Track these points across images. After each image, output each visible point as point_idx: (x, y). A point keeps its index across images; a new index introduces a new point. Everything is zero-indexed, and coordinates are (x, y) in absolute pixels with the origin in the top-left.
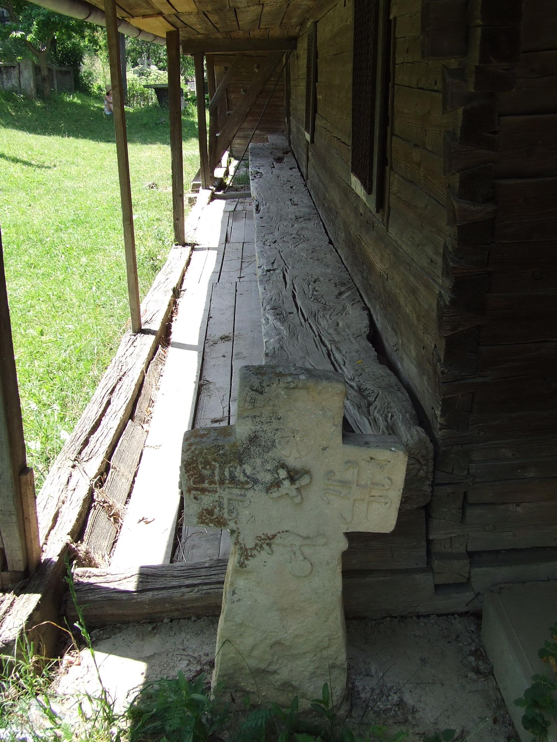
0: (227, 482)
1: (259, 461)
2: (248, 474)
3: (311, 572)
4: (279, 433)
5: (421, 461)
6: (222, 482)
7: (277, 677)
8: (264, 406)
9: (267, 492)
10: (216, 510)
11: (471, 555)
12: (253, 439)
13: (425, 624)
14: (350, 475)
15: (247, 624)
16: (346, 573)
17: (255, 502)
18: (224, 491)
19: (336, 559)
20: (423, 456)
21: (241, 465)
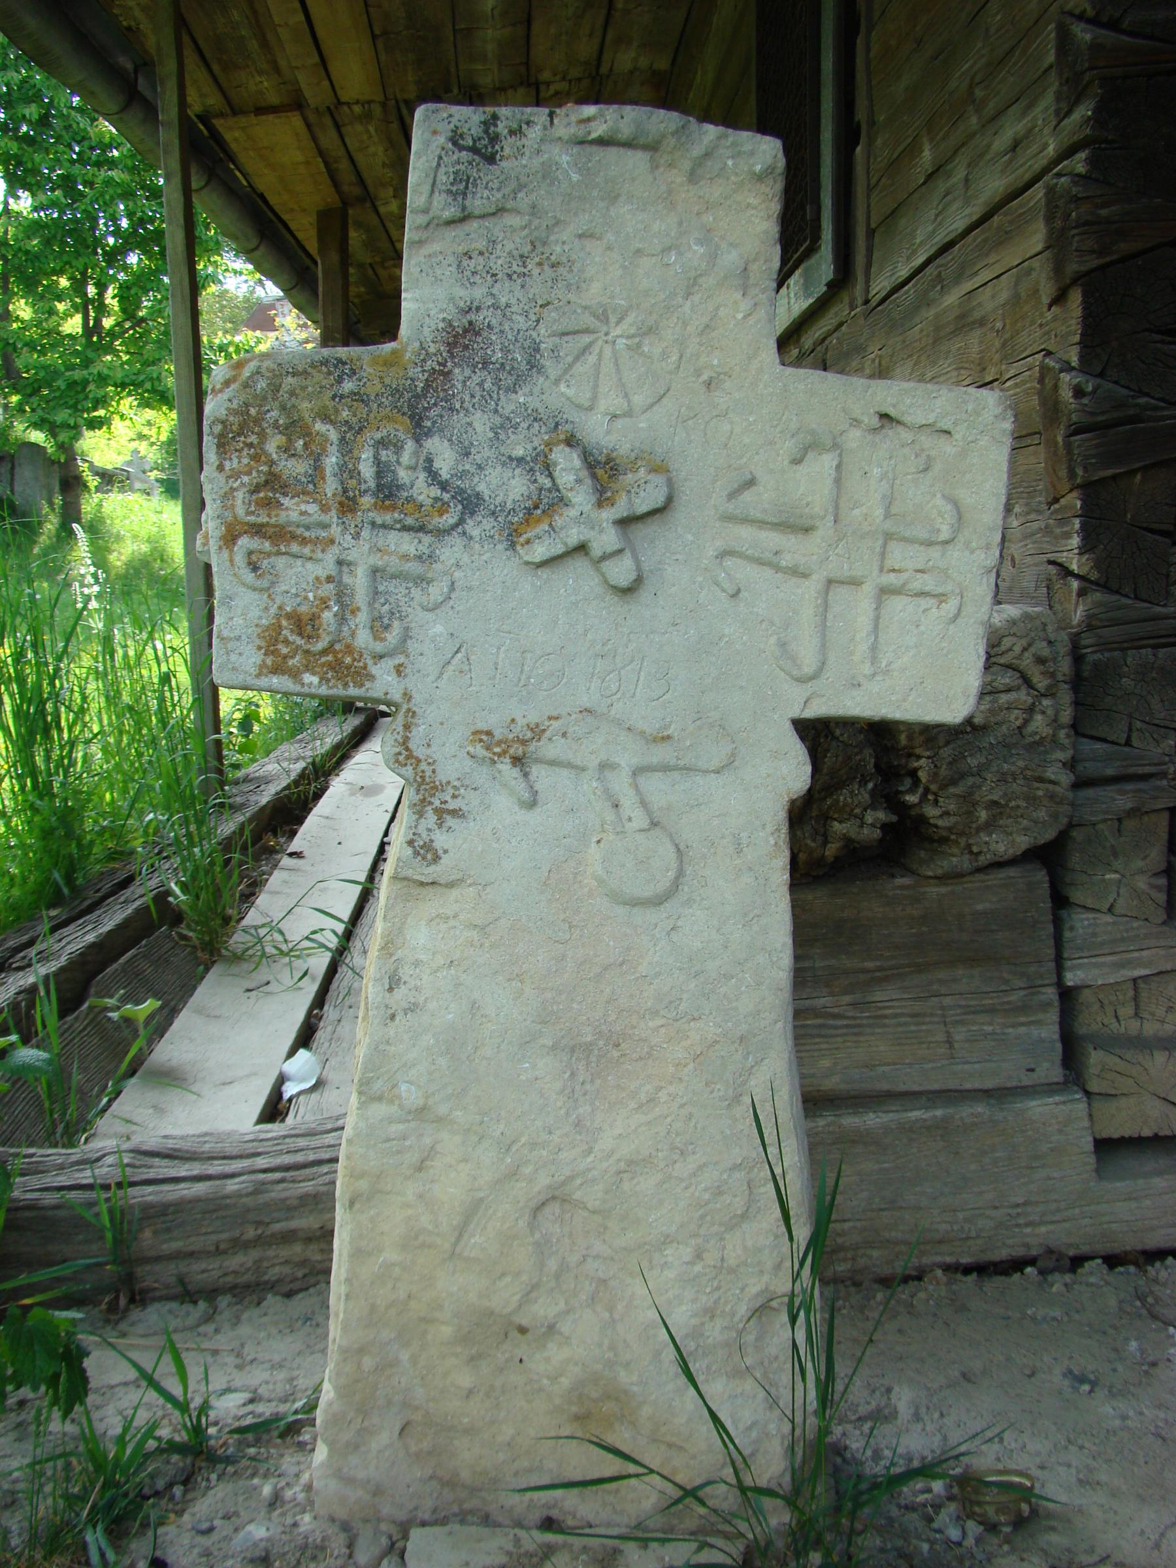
0: (367, 501)
1: (481, 423)
2: (445, 475)
3: (676, 884)
4: (550, 315)
5: (1035, 680)
6: (347, 505)
7: (556, 1353)
8: (500, 211)
9: (512, 546)
10: (327, 616)
14: (812, 483)
15: (443, 1110)
16: (806, 872)
17: (470, 589)
18: (356, 537)
19: (770, 828)
20: (1041, 661)
21: (418, 441)
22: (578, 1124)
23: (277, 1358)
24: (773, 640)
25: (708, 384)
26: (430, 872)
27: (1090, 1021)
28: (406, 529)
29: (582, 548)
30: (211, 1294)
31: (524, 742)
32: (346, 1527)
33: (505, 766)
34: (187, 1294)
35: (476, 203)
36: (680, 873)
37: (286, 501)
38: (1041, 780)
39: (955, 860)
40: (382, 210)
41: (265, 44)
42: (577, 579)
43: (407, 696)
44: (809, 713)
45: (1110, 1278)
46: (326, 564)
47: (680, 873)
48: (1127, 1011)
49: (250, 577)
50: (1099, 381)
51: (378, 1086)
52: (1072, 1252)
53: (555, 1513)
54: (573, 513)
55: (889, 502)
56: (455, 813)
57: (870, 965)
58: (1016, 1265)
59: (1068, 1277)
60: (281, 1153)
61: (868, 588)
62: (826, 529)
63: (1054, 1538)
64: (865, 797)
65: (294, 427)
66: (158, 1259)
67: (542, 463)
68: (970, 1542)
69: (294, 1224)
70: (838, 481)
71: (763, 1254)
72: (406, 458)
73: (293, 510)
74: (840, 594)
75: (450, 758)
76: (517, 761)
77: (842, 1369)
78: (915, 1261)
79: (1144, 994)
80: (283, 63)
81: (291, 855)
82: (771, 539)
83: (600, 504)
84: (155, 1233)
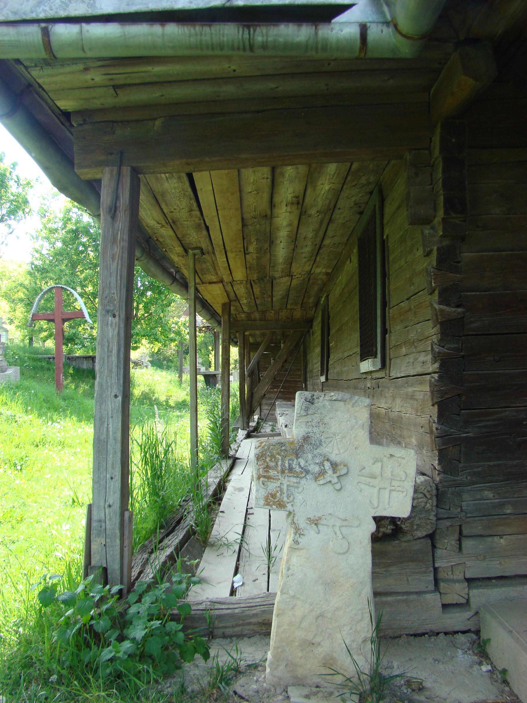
0: (287, 471)
1: (310, 456)
2: (302, 466)
3: (348, 550)
4: (324, 434)
6: (283, 472)
7: (320, 649)
8: (314, 413)
9: (316, 481)
10: (278, 494)
11: (469, 580)
12: (306, 439)
13: (435, 639)
14: (376, 469)
15: (298, 596)
18: (284, 478)
20: (428, 491)
21: (297, 459)
22: (326, 600)
23: (249, 652)
24: (368, 500)
25: (355, 448)
26: (297, 546)
27: (441, 575)
28: (294, 477)
29: (330, 482)
30: (231, 637)
31: (317, 520)
32: (273, 686)
33: (313, 525)
34: (224, 636)
35: (310, 412)
36: (349, 548)
37: (270, 471)
38: (429, 519)
39: (409, 537)
40: (241, 302)
41: (215, 269)
42: (329, 487)
43: (294, 511)
44: (375, 515)
45: (445, 638)
46: (278, 484)
47: (349, 548)
48: (450, 573)
49: (262, 486)
50: (442, 426)
51: (285, 591)
52: (437, 631)
53: (319, 685)
54: (328, 475)
55: (392, 472)
56: (303, 535)
57: (389, 561)
58: (423, 634)
59: (435, 637)
60: (246, 603)
61: (388, 490)
62: (379, 478)
63: (427, 693)
64: (388, 523)
65: (272, 456)
66: (218, 628)
67: (322, 464)
68: (409, 693)
69: (251, 620)
70: (382, 468)
71: (366, 628)
72: (295, 463)
73: (272, 473)
74: (382, 491)
75: (302, 523)
76: (316, 524)
77: (381, 657)
78: (399, 633)
79: (454, 569)
80: (219, 273)
81: (221, 512)
82: (368, 480)
83: (334, 473)
84: (218, 621)
